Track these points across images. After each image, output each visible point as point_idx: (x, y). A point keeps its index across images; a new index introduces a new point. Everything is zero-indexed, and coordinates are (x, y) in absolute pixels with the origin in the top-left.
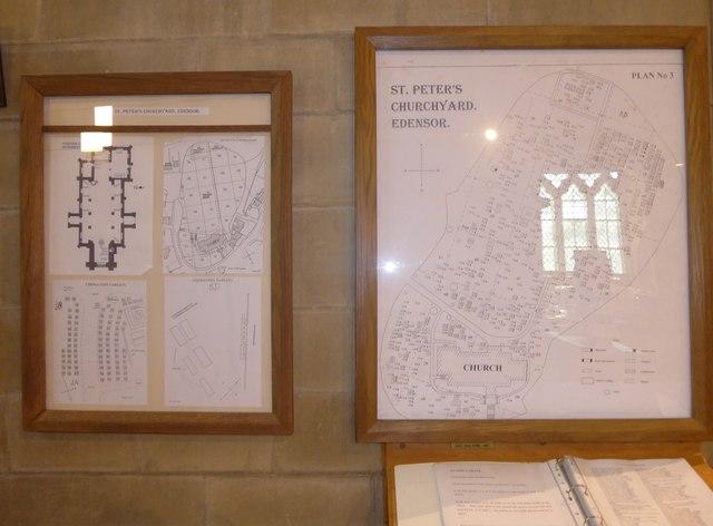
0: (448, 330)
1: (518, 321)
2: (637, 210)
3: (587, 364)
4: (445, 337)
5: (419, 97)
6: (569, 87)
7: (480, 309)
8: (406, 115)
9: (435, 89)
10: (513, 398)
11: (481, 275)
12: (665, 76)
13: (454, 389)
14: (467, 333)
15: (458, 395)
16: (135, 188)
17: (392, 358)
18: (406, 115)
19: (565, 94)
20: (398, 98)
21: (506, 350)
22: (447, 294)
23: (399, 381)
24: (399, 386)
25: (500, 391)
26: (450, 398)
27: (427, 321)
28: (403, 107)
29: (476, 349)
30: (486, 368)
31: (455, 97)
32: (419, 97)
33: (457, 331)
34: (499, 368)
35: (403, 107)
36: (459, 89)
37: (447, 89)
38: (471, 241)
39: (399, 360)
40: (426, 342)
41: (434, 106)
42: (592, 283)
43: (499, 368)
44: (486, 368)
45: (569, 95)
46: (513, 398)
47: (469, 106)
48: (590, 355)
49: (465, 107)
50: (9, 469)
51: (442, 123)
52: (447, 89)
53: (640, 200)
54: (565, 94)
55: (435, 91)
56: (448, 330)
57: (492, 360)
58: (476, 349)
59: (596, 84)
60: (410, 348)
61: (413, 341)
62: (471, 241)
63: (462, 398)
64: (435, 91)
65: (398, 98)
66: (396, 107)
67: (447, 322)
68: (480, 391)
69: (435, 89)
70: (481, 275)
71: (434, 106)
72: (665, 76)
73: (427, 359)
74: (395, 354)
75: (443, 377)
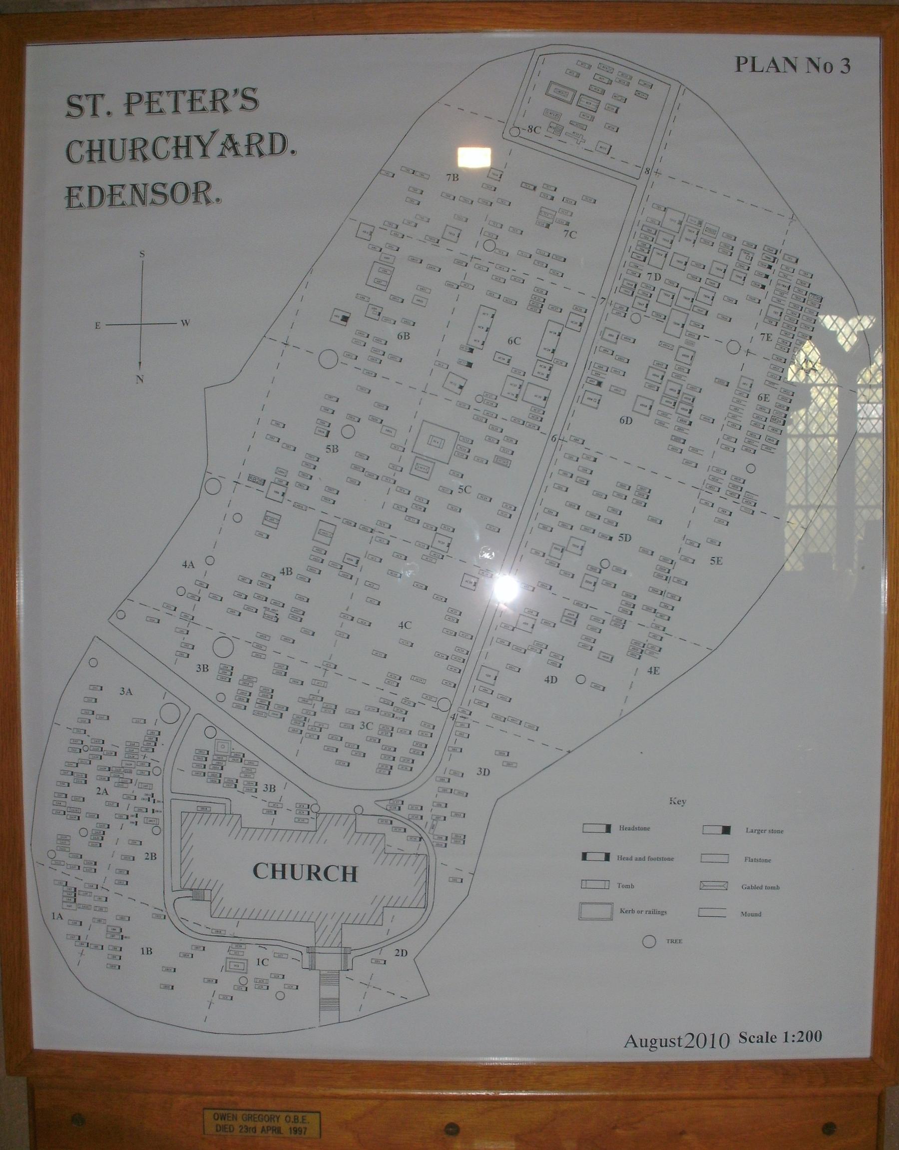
0: (210, 766)
1: (403, 744)
2: (741, 436)
3: (596, 868)
4: (203, 787)
5: (142, 125)
6: (556, 91)
7: (297, 709)
8: (104, 174)
9: (184, 100)
10: (389, 953)
11: (298, 616)
12: (828, 68)
13: (229, 927)
14: (263, 776)
15: (239, 944)
16: (422, 681)
17: (64, 840)
18: (104, 174)
19: (548, 112)
20: (89, 129)
21: (367, 824)
22: (205, 668)
23: (80, 899)
24: (86, 916)
25: (354, 937)
26: (218, 952)
27: (153, 741)
28: (97, 151)
29: (285, 819)
30: (313, 873)
31: (239, 123)
32: (142, 125)
33: (232, 770)
34: (350, 874)
35: (97, 151)
36: (249, 98)
37: (219, 101)
38: (272, 519)
39: (80, 845)
40: (151, 798)
41: (182, 148)
42: (614, 640)
43: (350, 874)
44: (313, 873)
45: (558, 115)
46: (389, 953)
47: (277, 144)
48: (599, 843)
49: (265, 147)
50: (815, 370)
51: (198, 192)
52: (219, 101)
53: (751, 406)
54: (548, 112)
55: (184, 105)
56: (210, 766)
57: (331, 849)
58: (285, 819)
59: (634, 86)
60: (108, 815)
61: (116, 794)
62: (272, 519)
63: (252, 953)
64: (184, 105)
65: (89, 129)
66: (78, 152)
67: (209, 745)
68: (304, 935)
69: (184, 100)
70: (298, 616)
71: (182, 148)
72: (828, 68)
73: (153, 844)
74: (71, 828)
75: (197, 895)
